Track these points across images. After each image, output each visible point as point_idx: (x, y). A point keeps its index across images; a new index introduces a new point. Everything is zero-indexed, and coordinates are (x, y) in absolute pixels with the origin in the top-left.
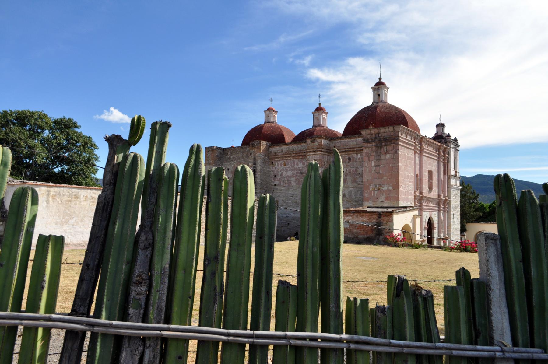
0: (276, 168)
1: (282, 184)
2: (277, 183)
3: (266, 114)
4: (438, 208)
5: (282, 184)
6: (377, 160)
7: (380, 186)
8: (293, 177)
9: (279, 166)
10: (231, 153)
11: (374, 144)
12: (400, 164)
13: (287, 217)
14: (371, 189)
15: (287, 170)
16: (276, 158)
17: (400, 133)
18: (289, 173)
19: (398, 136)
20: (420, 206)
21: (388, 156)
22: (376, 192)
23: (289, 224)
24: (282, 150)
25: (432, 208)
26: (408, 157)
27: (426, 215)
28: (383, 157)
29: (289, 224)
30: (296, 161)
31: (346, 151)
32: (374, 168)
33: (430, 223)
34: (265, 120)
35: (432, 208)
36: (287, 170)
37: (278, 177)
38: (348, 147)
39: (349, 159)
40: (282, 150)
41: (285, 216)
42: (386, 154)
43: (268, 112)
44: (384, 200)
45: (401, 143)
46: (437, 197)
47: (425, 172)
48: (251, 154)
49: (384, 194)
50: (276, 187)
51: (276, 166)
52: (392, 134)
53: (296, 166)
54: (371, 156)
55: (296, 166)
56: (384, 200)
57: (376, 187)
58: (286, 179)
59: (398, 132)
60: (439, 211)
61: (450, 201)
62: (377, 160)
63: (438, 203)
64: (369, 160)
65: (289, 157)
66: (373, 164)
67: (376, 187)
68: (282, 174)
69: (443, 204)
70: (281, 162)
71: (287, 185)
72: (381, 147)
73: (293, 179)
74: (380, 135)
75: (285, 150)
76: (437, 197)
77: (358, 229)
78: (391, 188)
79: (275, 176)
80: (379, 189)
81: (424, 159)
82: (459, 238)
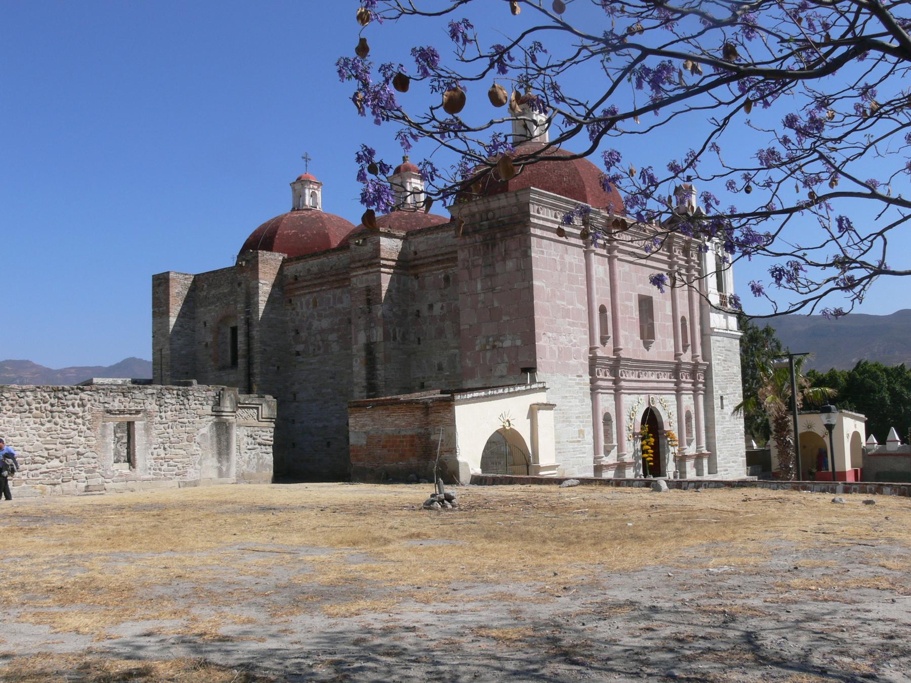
0: (298, 314)
1: (311, 348)
2: (300, 348)
3: (294, 190)
4: (676, 384)
5: (311, 348)
6: (487, 276)
7: (497, 339)
8: (332, 330)
9: (305, 309)
10: (209, 285)
11: (478, 238)
12: (536, 283)
13: (325, 427)
14: (477, 348)
15: (320, 315)
16: (297, 289)
17: (533, 210)
18: (325, 324)
19: (528, 215)
20: (615, 382)
21: (510, 264)
22: (488, 354)
23: (328, 444)
24: (309, 270)
25: (655, 385)
26: (563, 264)
27: (634, 406)
28: (499, 269)
29: (328, 444)
30: (338, 292)
31: (438, 262)
32: (481, 297)
33: (651, 419)
34: (294, 204)
35: (655, 385)
36: (320, 315)
37: (303, 334)
38: (444, 250)
39: (447, 279)
40: (309, 270)
41: (320, 425)
42: (504, 260)
43: (298, 186)
44: (505, 372)
45: (538, 232)
46: (672, 360)
47: (629, 298)
48: (239, 284)
49: (506, 359)
50: (300, 359)
51: (299, 310)
52: (515, 210)
53: (339, 306)
54: (475, 266)
55: (339, 306)
56: (505, 373)
57: (488, 342)
58: (319, 337)
59: (528, 204)
60: (678, 392)
61: (709, 367)
62: (487, 276)
63: (676, 370)
64: (471, 278)
65: (322, 284)
66: (479, 287)
67: (488, 342)
68: (309, 328)
69: (694, 375)
70: (308, 297)
71: (322, 350)
72: (494, 245)
73: (333, 337)
74: (490, 215)
75: (315, 269)
76: (672, 360)
77: (384, 447)
78: (519, 342)
79: (297, 332)
80: (494, 347)
81: (621, 268)
82: (590, 462)
